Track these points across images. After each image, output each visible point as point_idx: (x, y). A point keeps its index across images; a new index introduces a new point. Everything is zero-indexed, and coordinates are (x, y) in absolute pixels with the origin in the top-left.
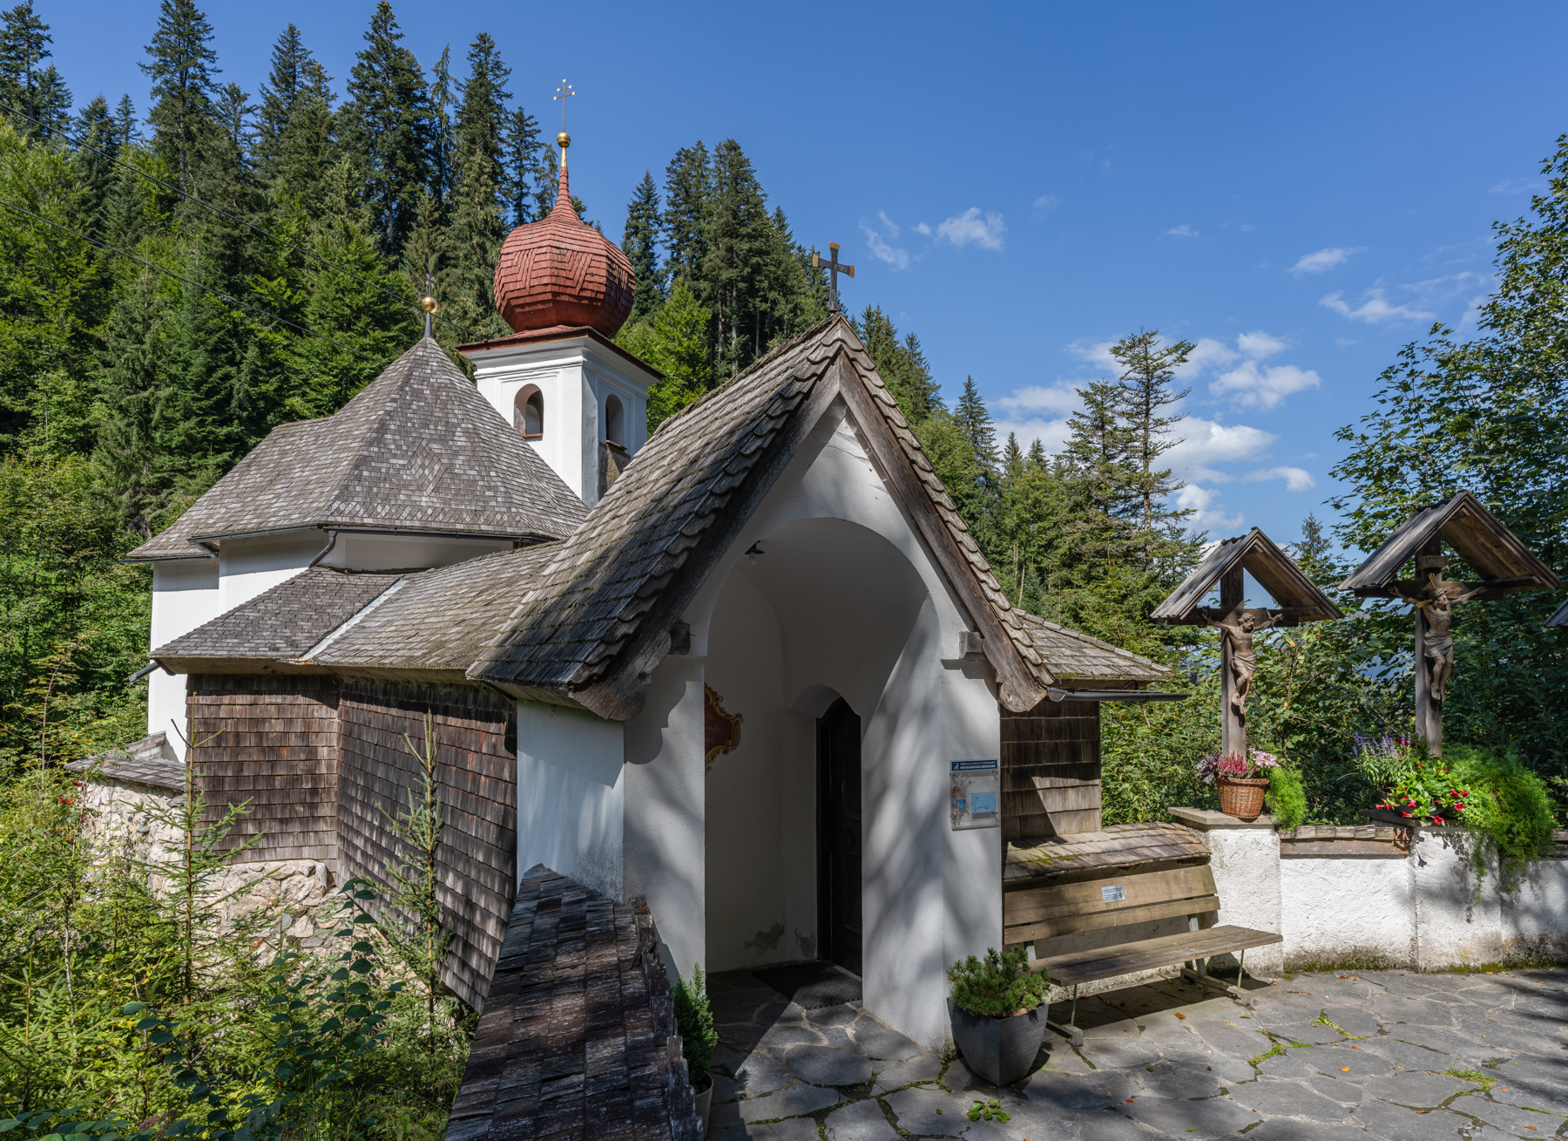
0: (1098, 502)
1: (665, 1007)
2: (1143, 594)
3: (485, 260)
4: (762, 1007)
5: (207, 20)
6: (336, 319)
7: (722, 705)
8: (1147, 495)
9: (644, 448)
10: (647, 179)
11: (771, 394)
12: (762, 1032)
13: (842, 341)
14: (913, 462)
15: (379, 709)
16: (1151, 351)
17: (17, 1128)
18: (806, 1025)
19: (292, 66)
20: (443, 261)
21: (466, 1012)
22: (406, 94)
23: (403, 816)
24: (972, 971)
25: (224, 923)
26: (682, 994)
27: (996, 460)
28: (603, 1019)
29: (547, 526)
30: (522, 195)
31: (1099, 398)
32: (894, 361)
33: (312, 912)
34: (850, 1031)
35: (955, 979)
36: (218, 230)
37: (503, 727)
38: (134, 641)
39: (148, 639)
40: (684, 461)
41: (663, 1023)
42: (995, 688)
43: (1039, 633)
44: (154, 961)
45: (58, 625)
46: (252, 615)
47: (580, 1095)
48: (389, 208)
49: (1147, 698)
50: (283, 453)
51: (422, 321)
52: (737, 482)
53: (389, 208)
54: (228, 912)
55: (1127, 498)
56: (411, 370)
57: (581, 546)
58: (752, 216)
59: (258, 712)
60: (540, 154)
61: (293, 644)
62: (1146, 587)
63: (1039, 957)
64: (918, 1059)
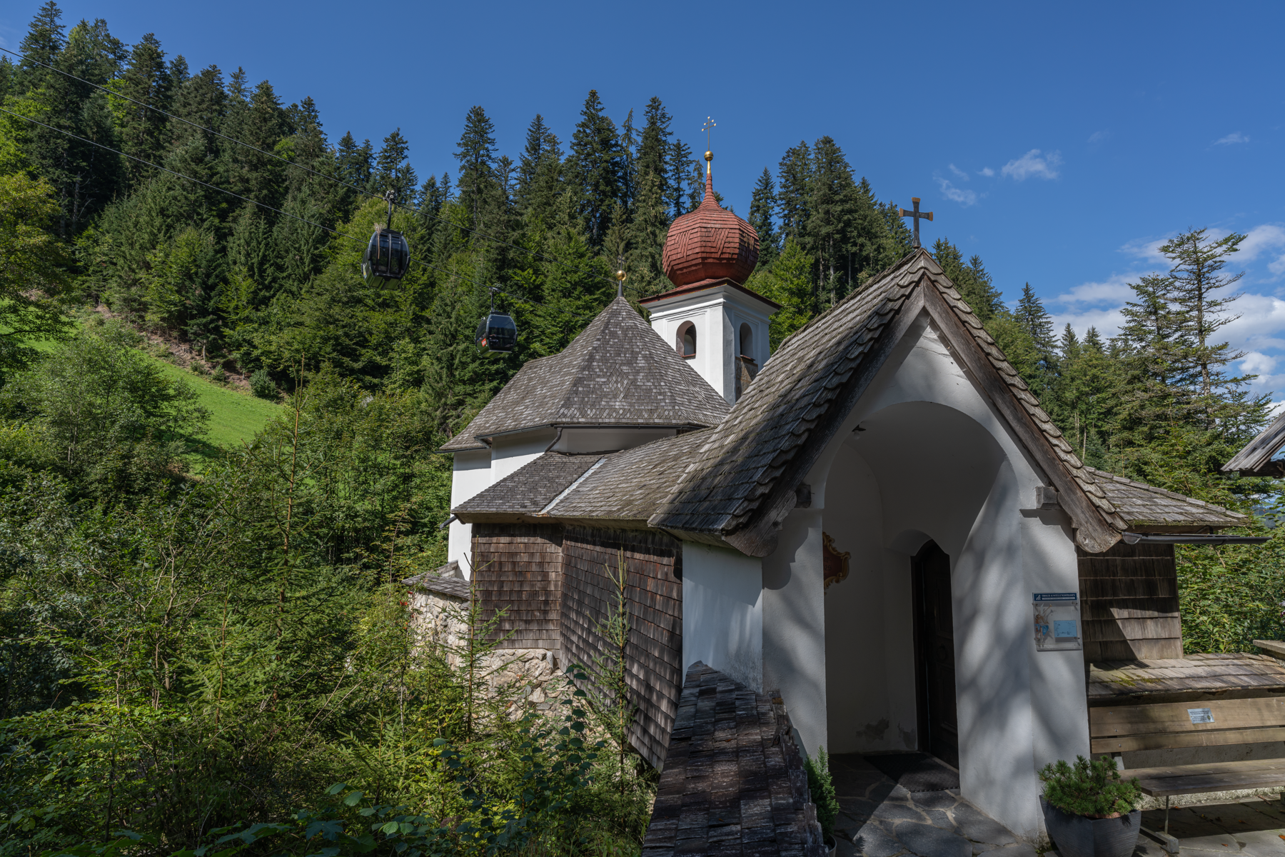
0: (1155, 375)
1: (801, 780)
2: (1207, 450)
3: (655, 242)
4: (873, 786)
5: (491, 122)
6: (561, 291)
7: (834, 545)
8: (1204, 366)
9: (771, 359)
10: (766, 173)
11: (869, 313)
12: (875, 807)
13: (925, 268)
14: (988, 354)
15: (589, 547)
16: (1200, 245)
17: (373, 815)
18: (911, 804)
19: (538, 139)
20: (629, 246)
21: (646, 766)
22: (606, 144)
23: (604, 621)
24: (1063, 774)
25: (490, 689)
26: (810, 770)
27: (1056, 347)
28: (755, 785)
29: (700, 418)
30: (680, 196)
31: (1151, 289)
32: (961, 278)
33: (544, 685)
34: (950, 815)
35: (1046, 779)
36: (494, 244)
37: (672, 560)
38: (441, 503)
39: (449, 500)
40: (802, 366)
41: (800, 793)
42: (1072, 533)
43: (1110, 486)
44: (450, 712)
45: (400, 493)
46: (511, 485)
47: (738, 841)
48: (595, 217)
49: (1224, 541)
50: (530, 379)
51: (615, 286)
52: (845, 379)
53: (595, 217)
54: (494, 682)
55: (1183, 370)
56: (609, 319)
57: (727, 432)
58: (842, 187)
59: (513, 549)
60: (692, 168)
61: (535, 503)
62: (1209, 444)
63: (1127, 767)
64: (1014, 846)
